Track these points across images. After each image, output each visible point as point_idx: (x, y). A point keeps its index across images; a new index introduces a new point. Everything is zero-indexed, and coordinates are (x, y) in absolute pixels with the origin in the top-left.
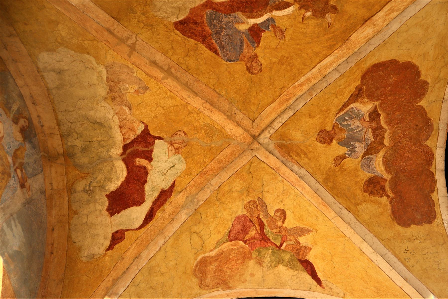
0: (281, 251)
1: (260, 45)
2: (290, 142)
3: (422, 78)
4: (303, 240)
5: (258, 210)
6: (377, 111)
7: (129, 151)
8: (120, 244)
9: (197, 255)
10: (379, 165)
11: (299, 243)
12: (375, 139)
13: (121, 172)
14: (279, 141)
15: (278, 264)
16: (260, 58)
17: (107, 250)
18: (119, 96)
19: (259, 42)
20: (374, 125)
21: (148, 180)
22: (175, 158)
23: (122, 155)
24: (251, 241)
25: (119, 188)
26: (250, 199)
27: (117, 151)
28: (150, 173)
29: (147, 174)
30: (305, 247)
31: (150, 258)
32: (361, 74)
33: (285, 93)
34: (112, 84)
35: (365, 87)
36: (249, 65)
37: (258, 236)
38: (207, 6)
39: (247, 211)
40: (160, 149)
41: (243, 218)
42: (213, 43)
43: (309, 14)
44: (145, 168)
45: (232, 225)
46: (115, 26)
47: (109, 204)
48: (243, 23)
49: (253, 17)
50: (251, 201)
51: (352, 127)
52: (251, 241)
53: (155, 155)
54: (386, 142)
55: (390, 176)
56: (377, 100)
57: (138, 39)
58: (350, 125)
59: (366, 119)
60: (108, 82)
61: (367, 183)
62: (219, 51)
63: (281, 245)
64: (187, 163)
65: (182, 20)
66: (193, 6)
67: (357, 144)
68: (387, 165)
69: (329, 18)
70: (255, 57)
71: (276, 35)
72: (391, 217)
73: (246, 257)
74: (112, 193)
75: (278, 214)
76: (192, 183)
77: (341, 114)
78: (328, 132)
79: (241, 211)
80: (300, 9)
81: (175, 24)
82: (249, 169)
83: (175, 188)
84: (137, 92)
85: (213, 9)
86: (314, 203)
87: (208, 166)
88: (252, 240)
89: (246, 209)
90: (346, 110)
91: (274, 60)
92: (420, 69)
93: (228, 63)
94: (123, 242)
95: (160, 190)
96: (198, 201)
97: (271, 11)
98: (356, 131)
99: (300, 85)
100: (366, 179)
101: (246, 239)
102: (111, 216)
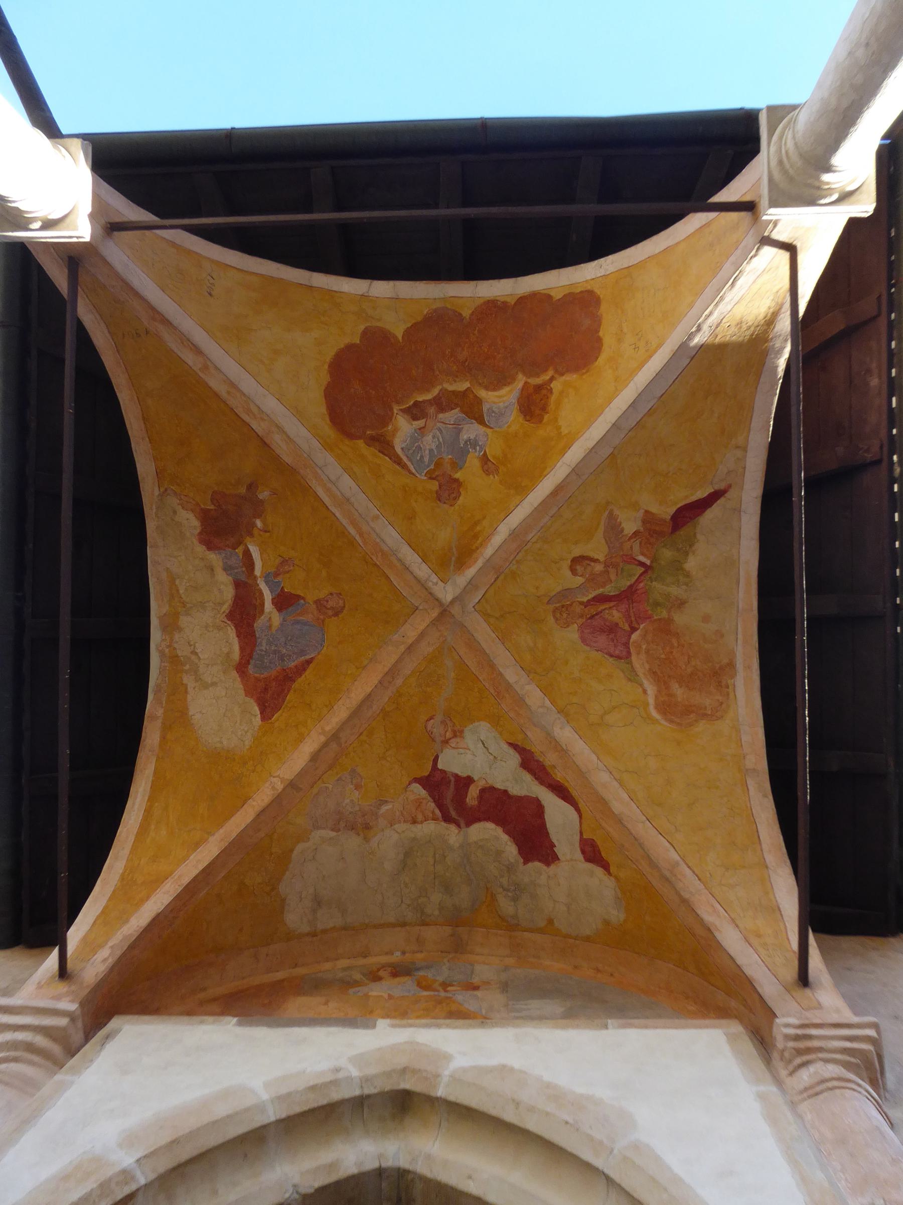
0: (654, 565)
1: (302, 595)
2: (454, 550)
3: (357, 341)
4: (630, 526)
5: (571, 605)
6: (409, 408)
7: (453, 814)
9: (649, 718)
10: (500, 397)
11: (636, 534)
12: (457, 405)
13: (487, 832)
14: (452, 568)
15: (682, 569)
16: (322, 596)
17: (609, 873)
18: (363, 816)
20: (432, 410)
21: (502, 788)
22: (469, 738)
23: (459, 826)
24: (633, 619)
25: (514, 838)
26: (551, 619)
27: (453, 834)
28: (491, 782)
29: (492, 789)
31: (628, 799)
32: (347, 442)
33: (374, 559)
34: (342, 824)
35: (368, 432)
36: (330, 613)
37: (623, 607)
38: (243, 672)
39: (573, 623)
40: (453, 762)
41: (586, 631)
42: (296, 666)
43: (259, 523)
44: (483, 791)
45: (598, 651)
46: (254, 803)
47: (540, 861)
49: (263, 605)
50: (554, 617)
51: (434, 448)
52: (633, 619)
53: (463, 773)
54: (462, 386)
56: (391, 410)
57: (277, 774)
58: (431, 451)
59: (422, 425)
60: (339, 830)
61: (528, 418)
62: (308, 657)
63: (642, 564)
64: (479, 720)
66: (243, 692)
67: (464, 436)
68: (501, 381)
69: (264, 494)
70: (318, 602)
71: (288, 572)
72: (583, 374)
73: (666, 628)
74: (521, 852)
75: (579, 569)
76: (512, 715)
77: (412, 468)
78: (440, 486)
79: (572, 634)
80: (251, 535)
82: (497, 618)
83: (519, 744)
84: (358, 787)
85: (248, 663)
86: (555, 509)
87: (487, 685)
88: (630, 617)
89: (568, 626)
90: (405, 459)
91: (324, 573)
92: (342, 346)
93: (326, 644)
94: (598, 843)
96: (543, 706)
97: (256, 577)
98: (441, 440)
99: (361, 535)
100: (521, 419)
101: (627, 627)
102: (558, 859)
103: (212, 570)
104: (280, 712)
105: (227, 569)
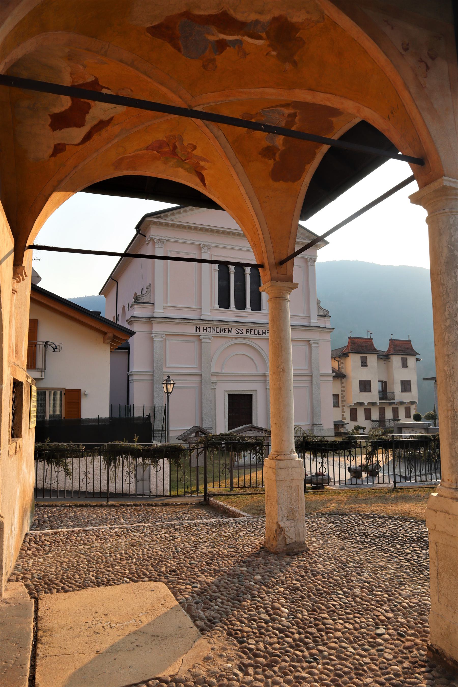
4: (202, 163)
8: (61, 154)
19: (222, 52)
30: (202, 167)
43: (274, 53)
44: (89, 104)
48: (213, 35)
49: (224, 33)
55: (284, 148)
65: (155, 26)
69: (288, 66)
70: (214, 60)
74: (55, 114)
81: (148, 28)
83: (113, 121)
95: (99, 120)
97: (243, 35)
103: (260, 13)
104: (151, 36)
105: (257, 22)
